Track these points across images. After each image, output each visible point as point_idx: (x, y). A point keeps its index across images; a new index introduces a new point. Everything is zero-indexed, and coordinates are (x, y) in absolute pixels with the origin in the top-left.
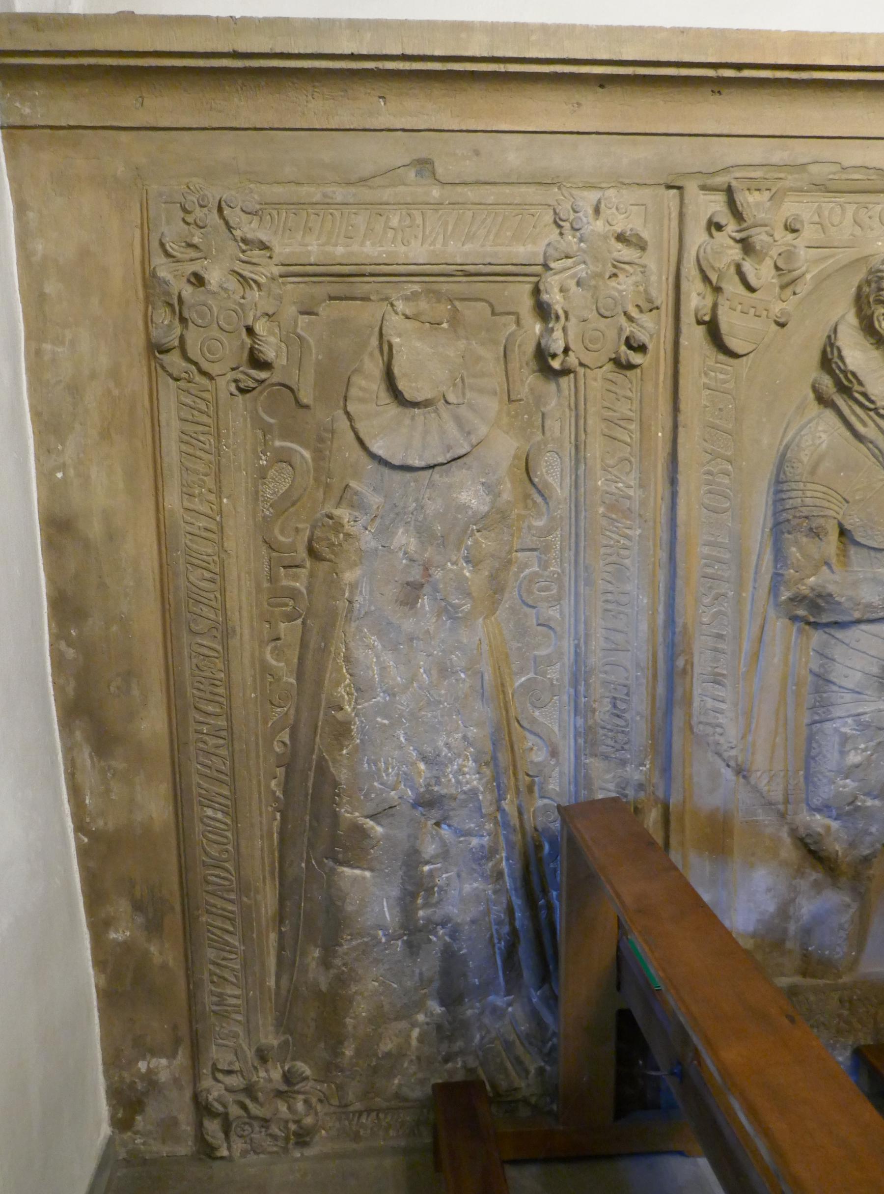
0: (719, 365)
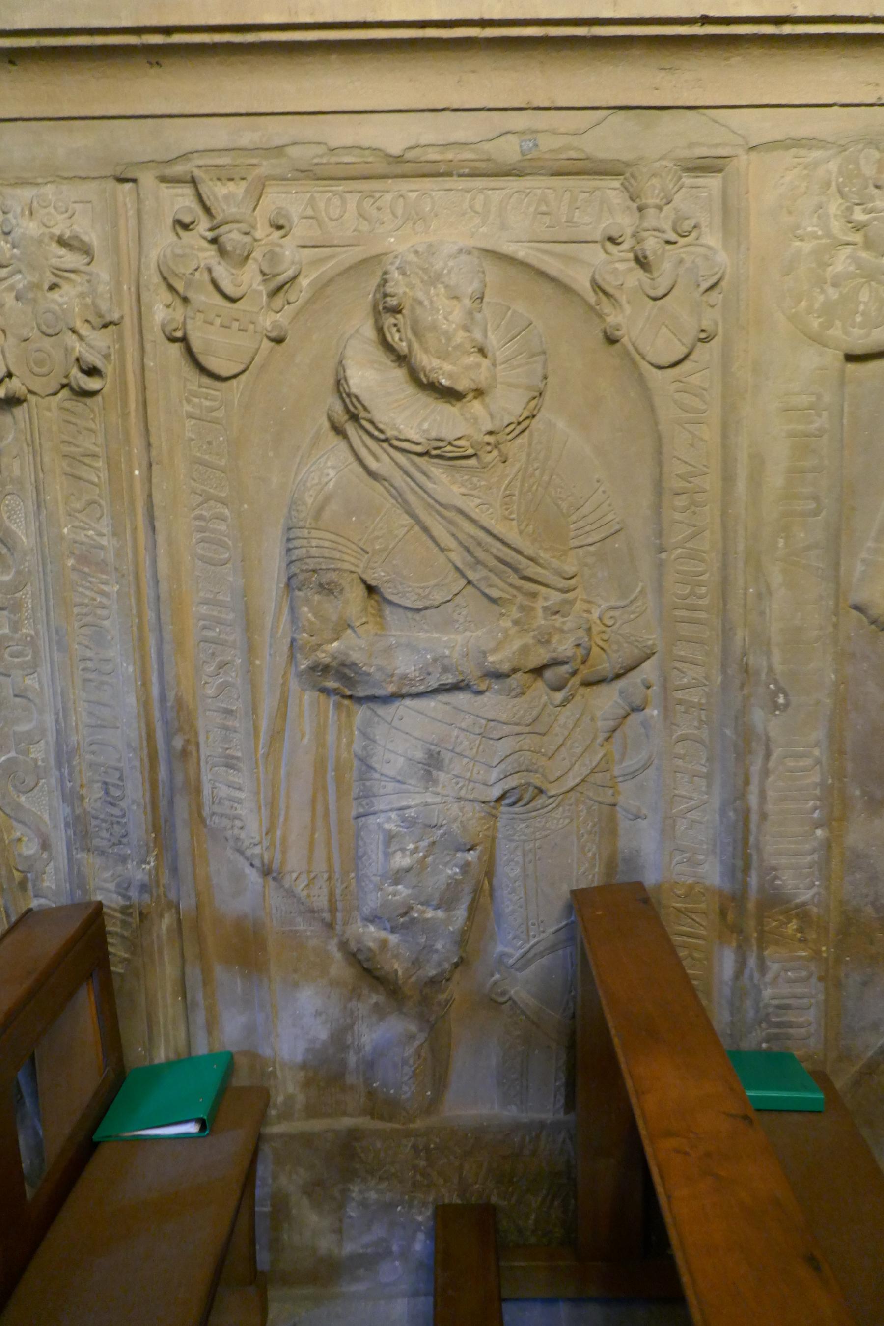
0: (204, 390)
